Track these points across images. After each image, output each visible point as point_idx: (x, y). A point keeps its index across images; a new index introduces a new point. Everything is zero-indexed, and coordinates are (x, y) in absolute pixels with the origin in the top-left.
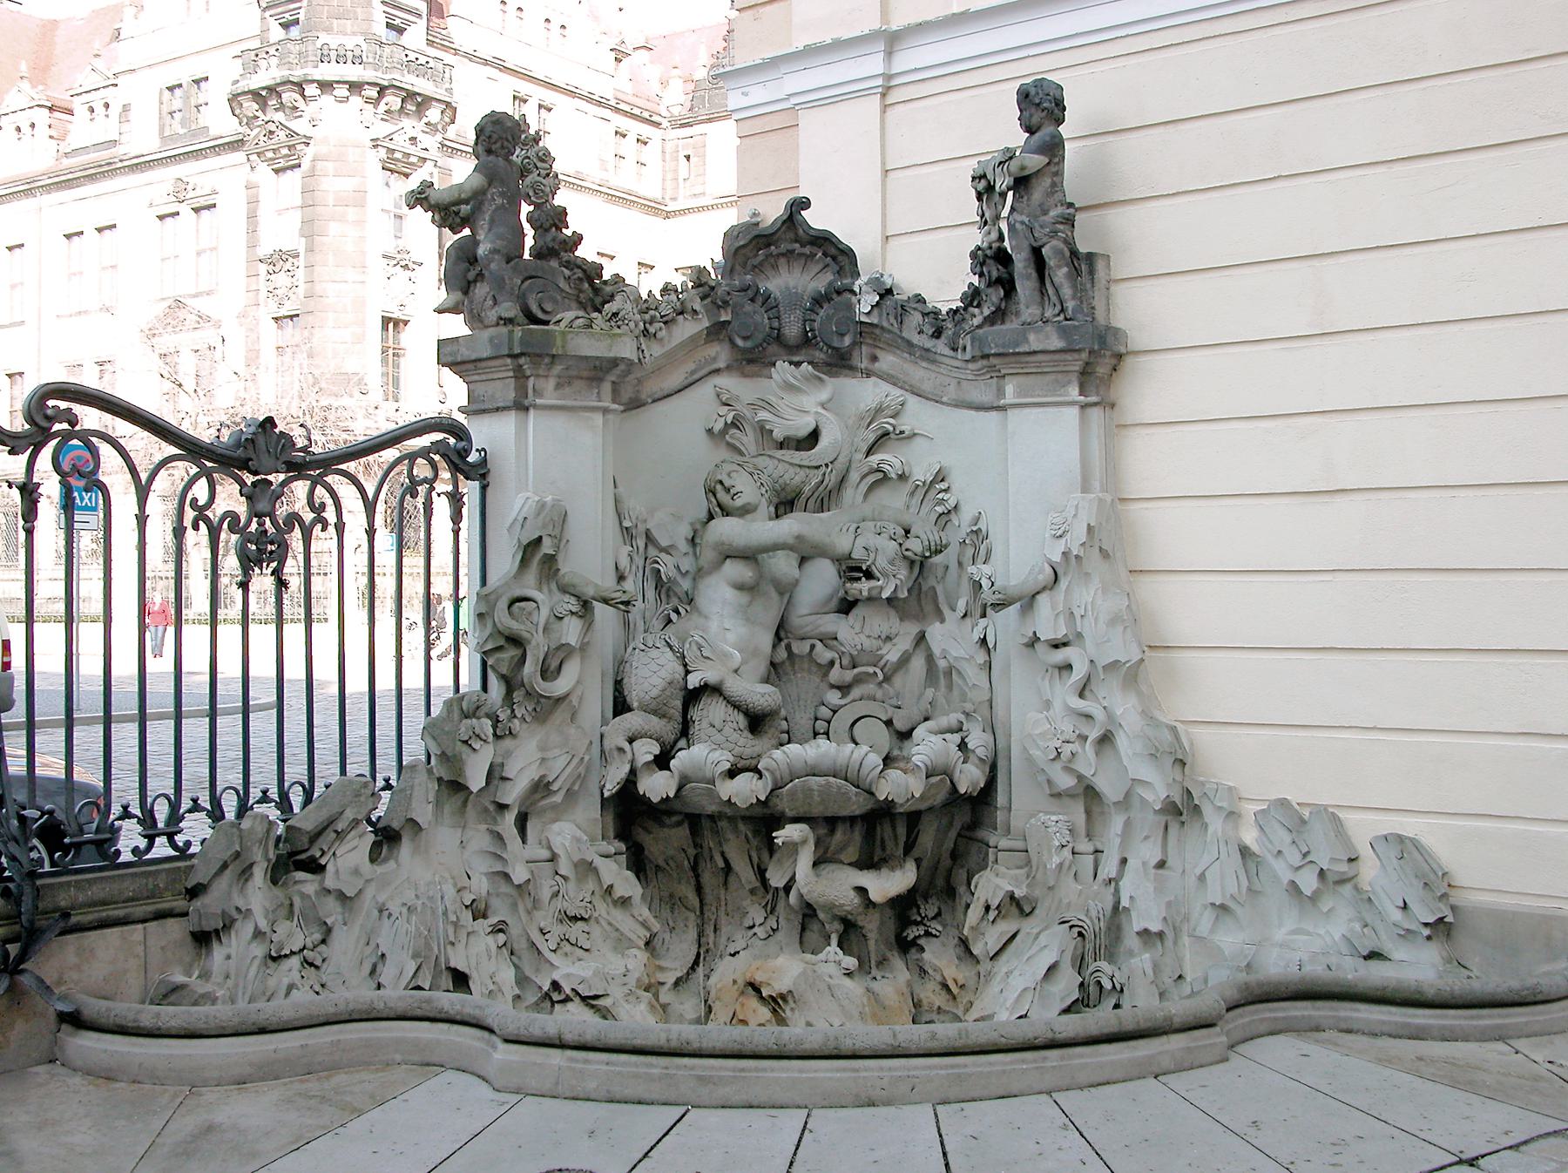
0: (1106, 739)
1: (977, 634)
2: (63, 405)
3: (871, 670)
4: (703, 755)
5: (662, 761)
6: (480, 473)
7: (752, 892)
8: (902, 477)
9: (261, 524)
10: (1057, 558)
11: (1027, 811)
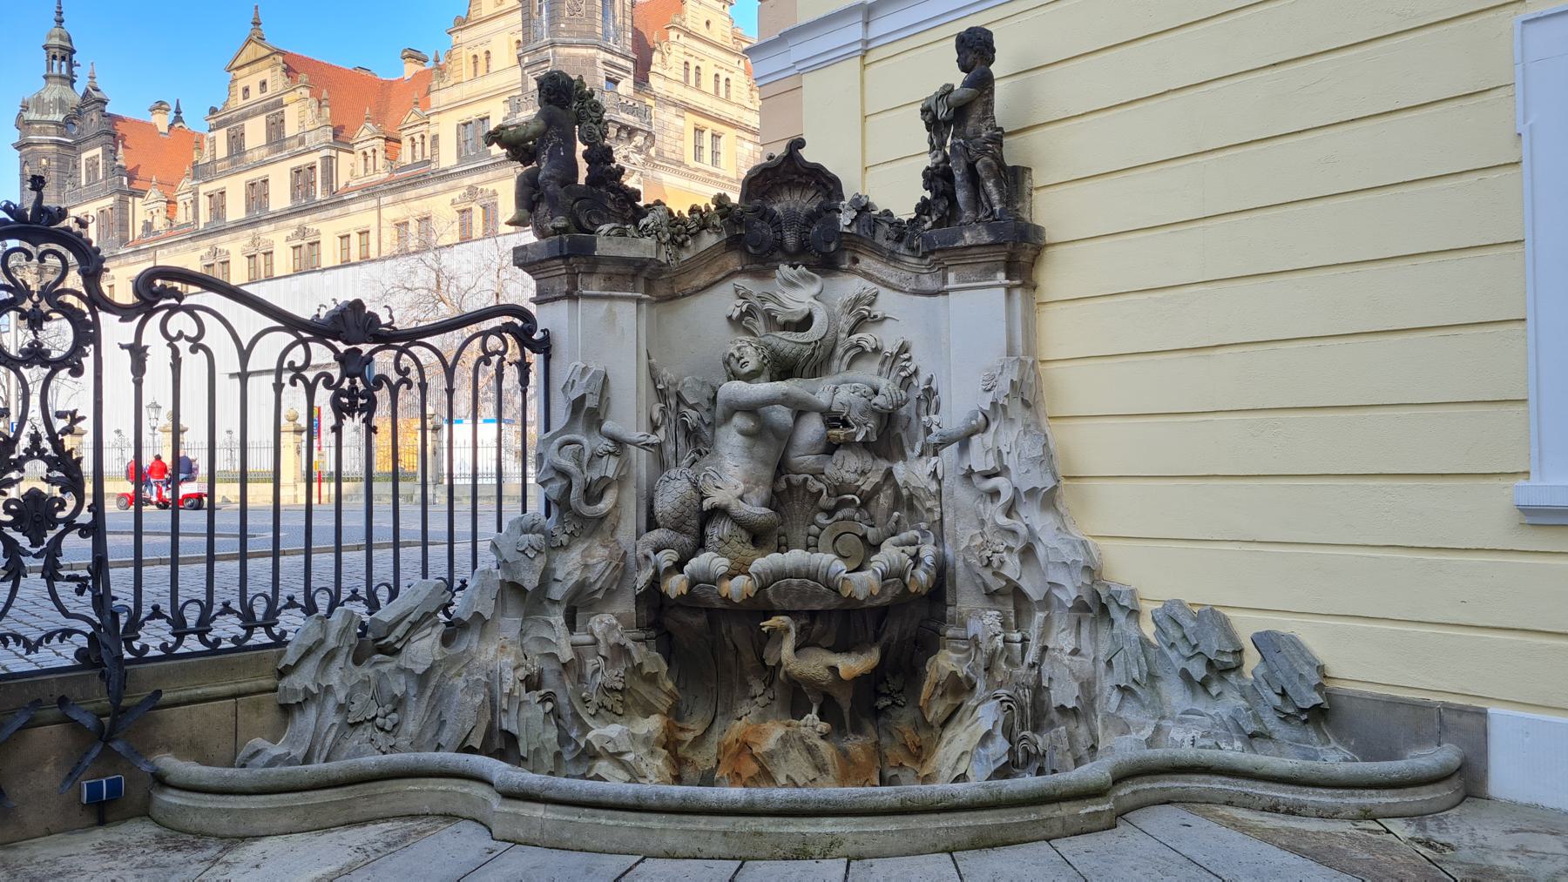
1: (929, 469)
4: (708, 561)
6: (545, 347)
8: (876, 351)
9: (353, 382)
10: (987, 407)
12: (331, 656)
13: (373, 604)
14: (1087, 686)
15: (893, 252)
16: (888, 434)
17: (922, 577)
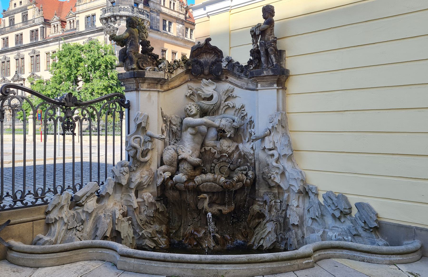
1: (251, 146)
3: (225, 154)
4: (181, 177)
6: (128, 106)
8: (233, 107)
10: (270, 128)
13: (75, 190)
14: (301, 218)
15: (239, 76)
16: (238, 134)
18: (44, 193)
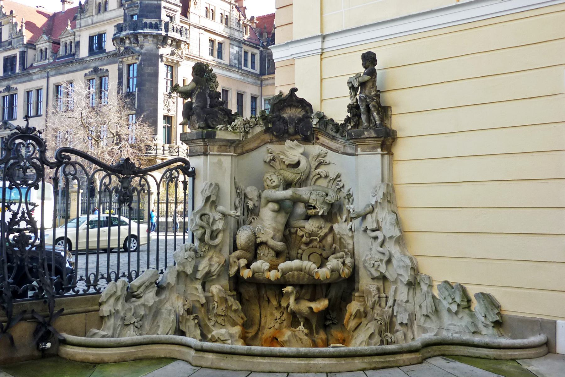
0: (389, 261)
1: (349, 227)
2: (67, 154)
3: (315, 238)
4: (261, 265)
5: (248, 266)
7: (276, 308)
8: (326, 177)
10: (373, 203)
11: (365, 282)
12: (118, 299)
15: (334, 136)
17: (346, 272)
18: (96, 280)
